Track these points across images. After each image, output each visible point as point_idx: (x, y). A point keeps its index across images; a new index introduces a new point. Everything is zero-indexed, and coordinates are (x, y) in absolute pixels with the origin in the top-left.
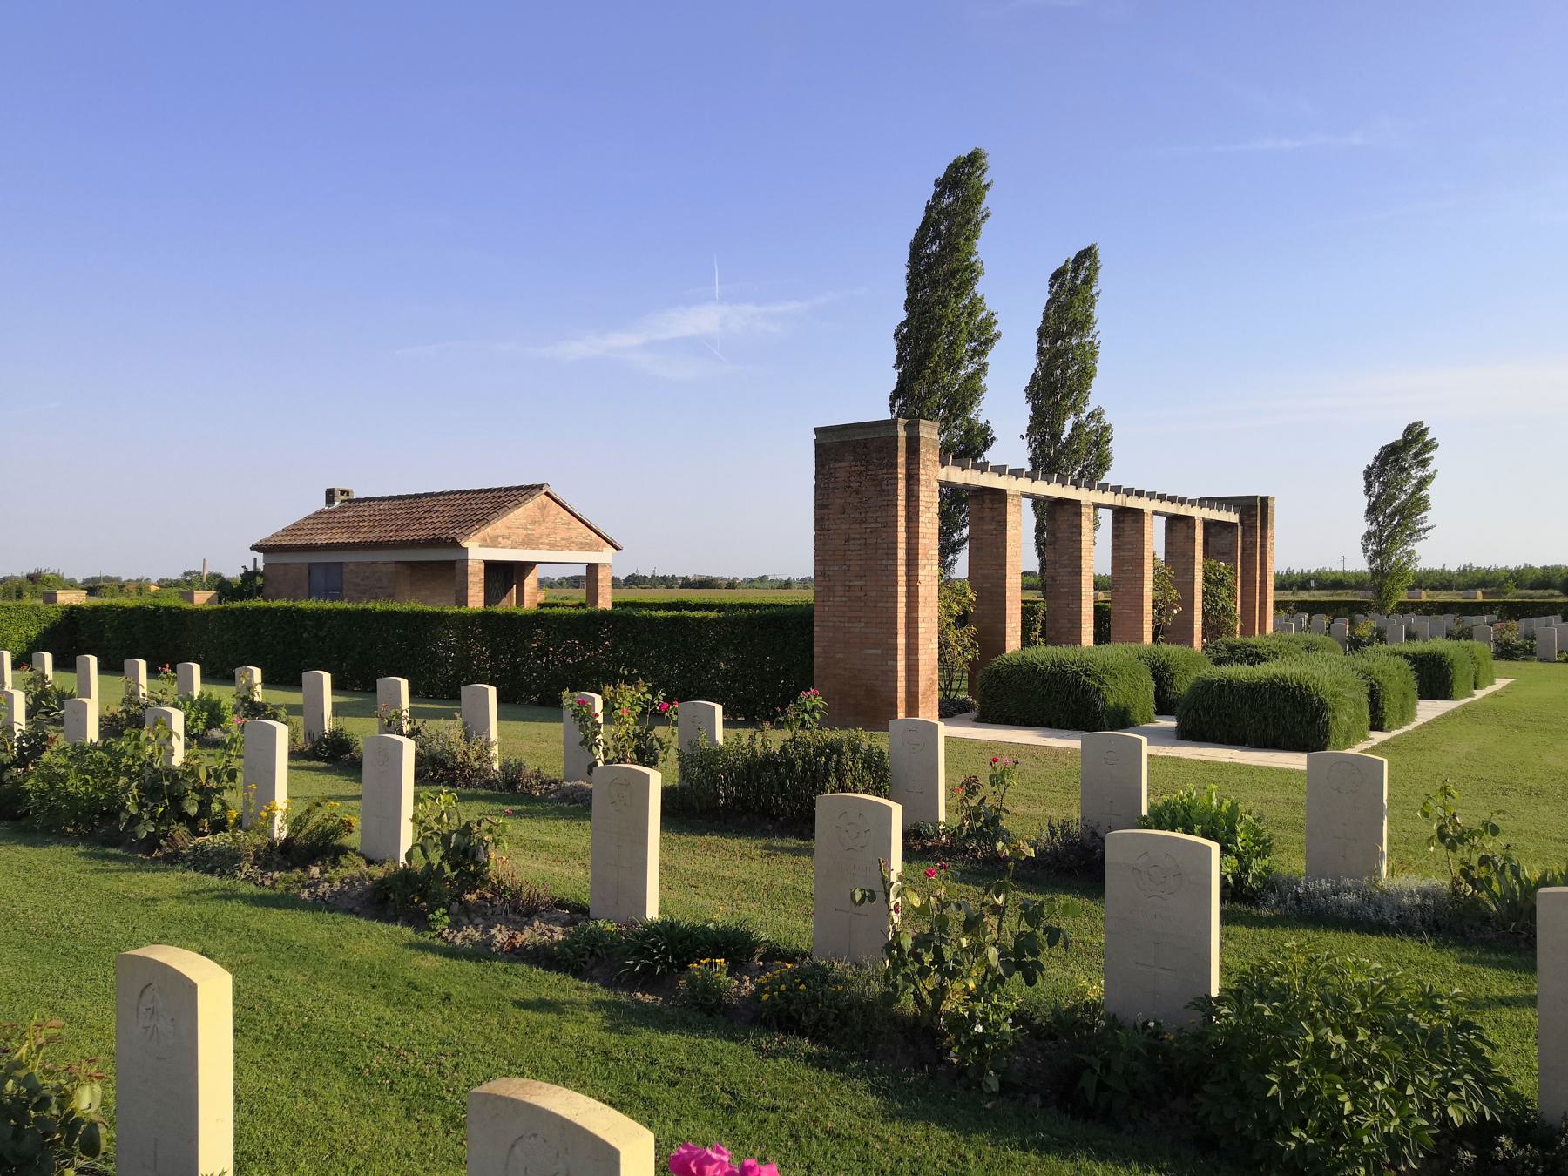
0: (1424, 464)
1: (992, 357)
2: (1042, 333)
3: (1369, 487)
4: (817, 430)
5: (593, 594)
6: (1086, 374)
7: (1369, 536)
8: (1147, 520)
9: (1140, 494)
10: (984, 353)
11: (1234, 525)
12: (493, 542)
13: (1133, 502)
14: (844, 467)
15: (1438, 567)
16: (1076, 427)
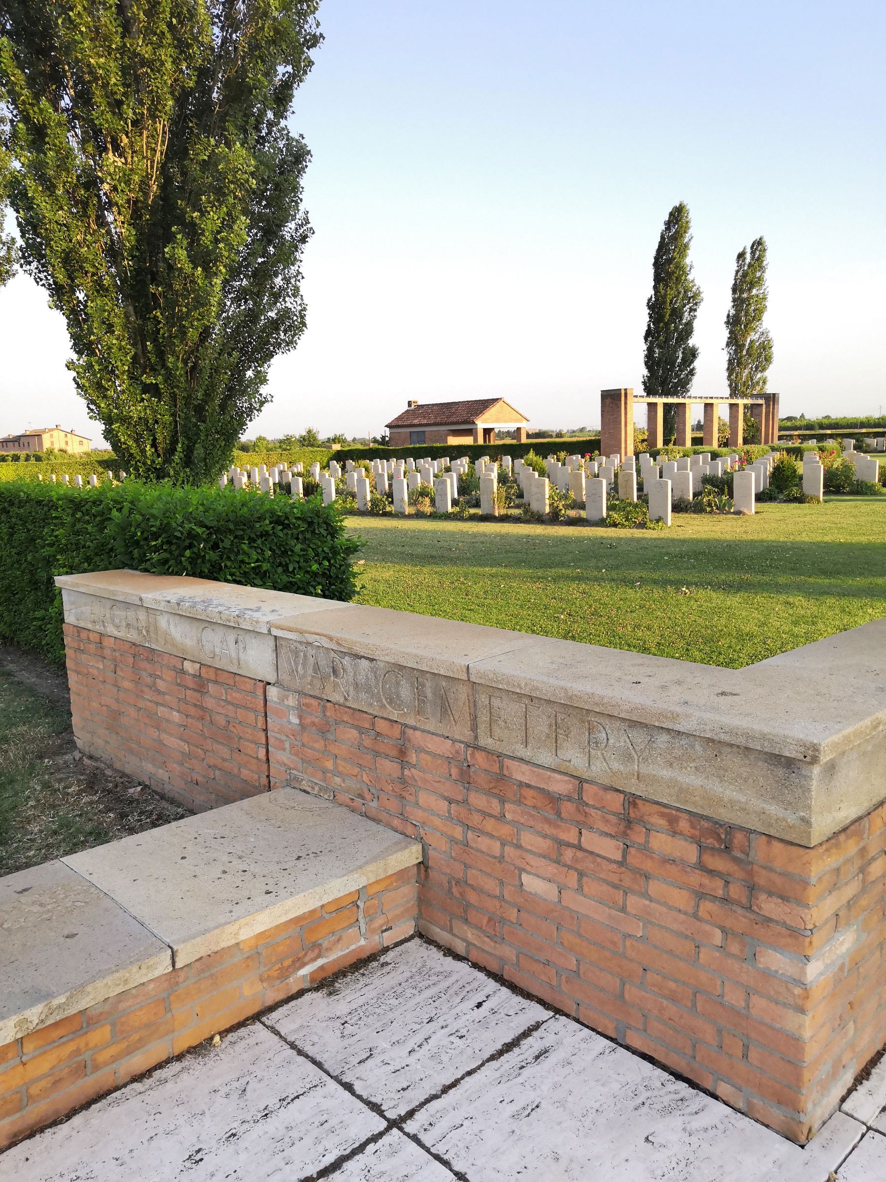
5: (519, 439)
9: (712, 398)
10: (695, 310)
12: (485, 421)
13: (709, 401)
14: (608, 401)
16: (751, 342)
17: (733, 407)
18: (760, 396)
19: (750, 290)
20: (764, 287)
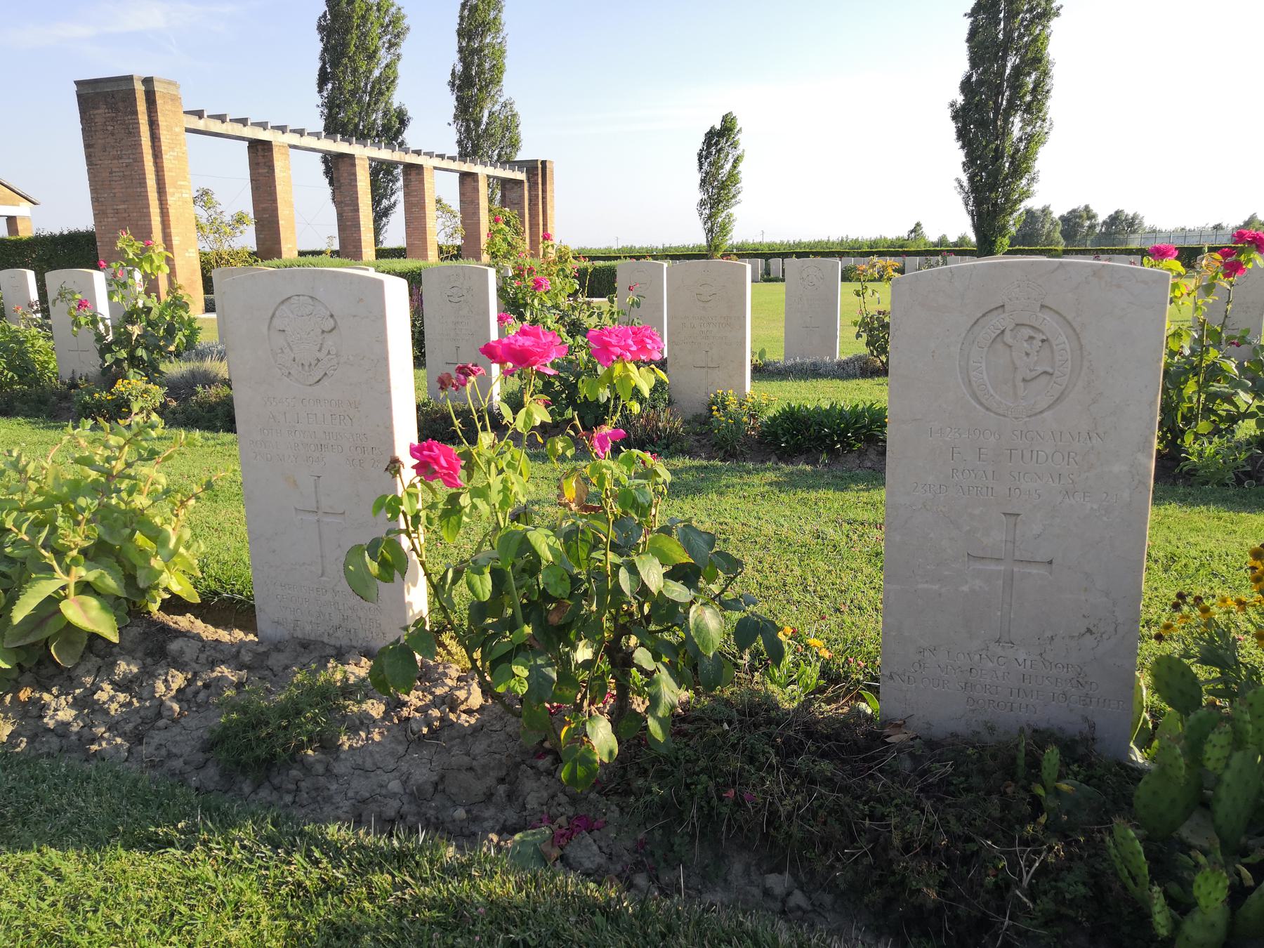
0: (734, 145)
1: (405, 47)
2: (461, 33)
3: (701, 165)
4: (77, 83)
6: (498, 69)
7: (702, 203)
8: (427, 175)
11: (522, 182)
14: (101, 113)
15: (825, 239)
16: (491, 114)
17: (467, 179)
18: (521, 165)
19: (483, 35)
20: (502, 35)
